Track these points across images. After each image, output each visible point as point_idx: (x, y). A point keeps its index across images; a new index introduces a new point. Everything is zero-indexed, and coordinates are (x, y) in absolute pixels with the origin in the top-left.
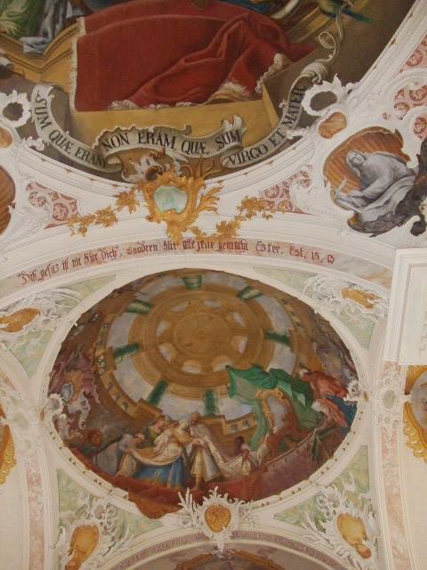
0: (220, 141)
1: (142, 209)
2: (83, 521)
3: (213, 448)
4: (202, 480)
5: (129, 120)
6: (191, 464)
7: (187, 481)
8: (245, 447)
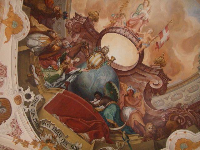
5: (55, 122)
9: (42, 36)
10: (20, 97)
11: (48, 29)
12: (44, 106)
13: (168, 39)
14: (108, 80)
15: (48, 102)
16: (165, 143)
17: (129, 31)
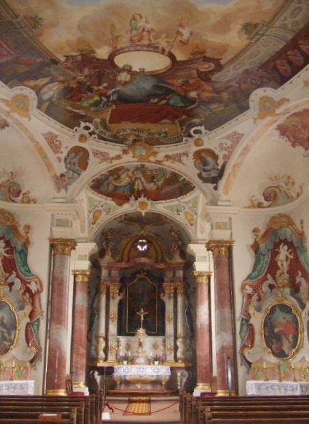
0: (160, 134)
1: (131, 154)
2: (97, 209)
3: (142, 179)
4: (138, 191)
5: (127, 127)
6: (134, 184)
7: (132, 191)
8: (155, 180)
9: (50, 85)
10: (82, 135)
11: (50, 78)
12: (107, 122)
13: (191, 33)
14: (148, 366)
15: (108, 118)
16: (248, 103)
17: (138, 45)
